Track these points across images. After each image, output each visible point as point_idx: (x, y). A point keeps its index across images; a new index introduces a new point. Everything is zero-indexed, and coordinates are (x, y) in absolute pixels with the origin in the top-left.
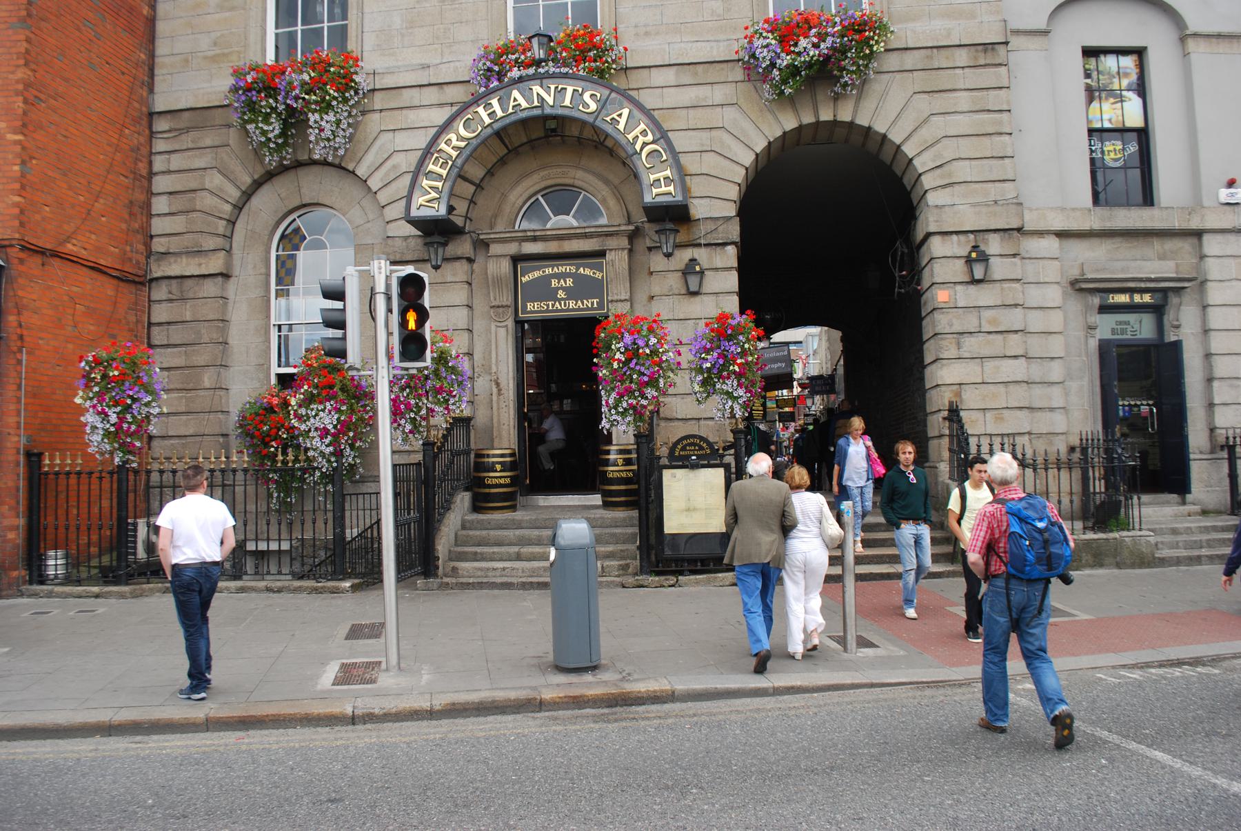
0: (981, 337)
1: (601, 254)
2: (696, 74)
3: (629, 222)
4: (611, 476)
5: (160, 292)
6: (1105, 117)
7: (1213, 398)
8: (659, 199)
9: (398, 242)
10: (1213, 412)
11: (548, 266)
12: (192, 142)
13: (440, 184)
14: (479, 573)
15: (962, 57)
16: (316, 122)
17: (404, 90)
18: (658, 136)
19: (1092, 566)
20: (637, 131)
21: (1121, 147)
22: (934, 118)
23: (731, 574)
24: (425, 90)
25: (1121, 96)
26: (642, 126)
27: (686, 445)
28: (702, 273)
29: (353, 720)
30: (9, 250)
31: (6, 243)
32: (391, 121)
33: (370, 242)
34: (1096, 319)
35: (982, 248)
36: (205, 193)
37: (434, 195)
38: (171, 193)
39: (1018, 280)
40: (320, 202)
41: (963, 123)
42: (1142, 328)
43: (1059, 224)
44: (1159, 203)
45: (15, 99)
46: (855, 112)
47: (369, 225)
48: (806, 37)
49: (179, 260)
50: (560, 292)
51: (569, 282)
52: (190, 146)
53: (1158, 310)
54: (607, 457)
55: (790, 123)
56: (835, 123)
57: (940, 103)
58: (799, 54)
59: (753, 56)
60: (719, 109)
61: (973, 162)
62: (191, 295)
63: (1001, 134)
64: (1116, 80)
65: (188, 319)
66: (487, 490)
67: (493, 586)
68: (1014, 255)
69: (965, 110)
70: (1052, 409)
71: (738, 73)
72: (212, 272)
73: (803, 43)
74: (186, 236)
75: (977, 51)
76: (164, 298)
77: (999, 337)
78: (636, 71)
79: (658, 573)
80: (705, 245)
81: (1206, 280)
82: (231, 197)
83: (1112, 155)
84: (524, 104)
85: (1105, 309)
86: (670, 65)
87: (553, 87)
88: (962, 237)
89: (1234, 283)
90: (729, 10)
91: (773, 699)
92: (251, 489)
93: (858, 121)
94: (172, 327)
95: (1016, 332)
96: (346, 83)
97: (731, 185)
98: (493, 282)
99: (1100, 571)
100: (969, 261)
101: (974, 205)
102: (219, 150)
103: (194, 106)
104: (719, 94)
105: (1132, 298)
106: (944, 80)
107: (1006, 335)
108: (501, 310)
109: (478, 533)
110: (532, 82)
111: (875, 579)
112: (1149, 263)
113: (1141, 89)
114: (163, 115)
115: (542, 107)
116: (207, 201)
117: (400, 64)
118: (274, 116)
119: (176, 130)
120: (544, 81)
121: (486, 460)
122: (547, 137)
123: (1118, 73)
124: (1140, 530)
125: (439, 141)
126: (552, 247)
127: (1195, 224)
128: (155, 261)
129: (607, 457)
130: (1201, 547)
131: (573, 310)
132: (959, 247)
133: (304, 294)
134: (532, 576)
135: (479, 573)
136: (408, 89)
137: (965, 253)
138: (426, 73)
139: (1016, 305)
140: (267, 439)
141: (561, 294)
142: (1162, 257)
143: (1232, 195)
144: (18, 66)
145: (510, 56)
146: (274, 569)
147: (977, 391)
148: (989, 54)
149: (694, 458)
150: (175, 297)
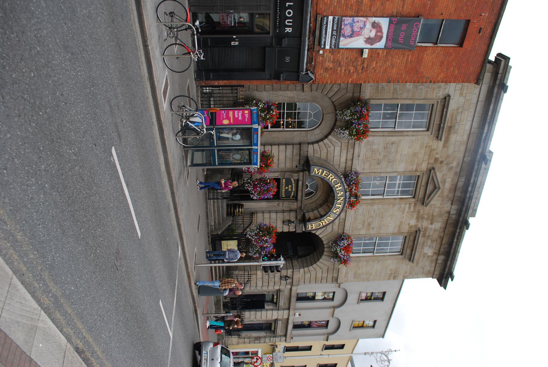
0: (268, 278)
2: (342, 222)
17: (353, 149)
22: (321, 270)
24: (352, 155)
26: (327, 222)
28: (288, 225)
37: (317, 172)
39: (280, 284)
40: (323, 121)
42: (268, 298)
47: (314, 136)
51: (290, 190)
53: (272, 301)
55: (325, 243)
60: (332, 227)
61: (309, 277)
68: (286, 284)
72: (304, 89)
77: (267, 281)
84: (338, 195)
87: (342, 202)
92: (231, 99)
100: (286, 276)
102: (346, 90)
113: (325, 299)
117: (362, 148)
125: (332, 173)
131: (282, 191)
141: (287, 188)
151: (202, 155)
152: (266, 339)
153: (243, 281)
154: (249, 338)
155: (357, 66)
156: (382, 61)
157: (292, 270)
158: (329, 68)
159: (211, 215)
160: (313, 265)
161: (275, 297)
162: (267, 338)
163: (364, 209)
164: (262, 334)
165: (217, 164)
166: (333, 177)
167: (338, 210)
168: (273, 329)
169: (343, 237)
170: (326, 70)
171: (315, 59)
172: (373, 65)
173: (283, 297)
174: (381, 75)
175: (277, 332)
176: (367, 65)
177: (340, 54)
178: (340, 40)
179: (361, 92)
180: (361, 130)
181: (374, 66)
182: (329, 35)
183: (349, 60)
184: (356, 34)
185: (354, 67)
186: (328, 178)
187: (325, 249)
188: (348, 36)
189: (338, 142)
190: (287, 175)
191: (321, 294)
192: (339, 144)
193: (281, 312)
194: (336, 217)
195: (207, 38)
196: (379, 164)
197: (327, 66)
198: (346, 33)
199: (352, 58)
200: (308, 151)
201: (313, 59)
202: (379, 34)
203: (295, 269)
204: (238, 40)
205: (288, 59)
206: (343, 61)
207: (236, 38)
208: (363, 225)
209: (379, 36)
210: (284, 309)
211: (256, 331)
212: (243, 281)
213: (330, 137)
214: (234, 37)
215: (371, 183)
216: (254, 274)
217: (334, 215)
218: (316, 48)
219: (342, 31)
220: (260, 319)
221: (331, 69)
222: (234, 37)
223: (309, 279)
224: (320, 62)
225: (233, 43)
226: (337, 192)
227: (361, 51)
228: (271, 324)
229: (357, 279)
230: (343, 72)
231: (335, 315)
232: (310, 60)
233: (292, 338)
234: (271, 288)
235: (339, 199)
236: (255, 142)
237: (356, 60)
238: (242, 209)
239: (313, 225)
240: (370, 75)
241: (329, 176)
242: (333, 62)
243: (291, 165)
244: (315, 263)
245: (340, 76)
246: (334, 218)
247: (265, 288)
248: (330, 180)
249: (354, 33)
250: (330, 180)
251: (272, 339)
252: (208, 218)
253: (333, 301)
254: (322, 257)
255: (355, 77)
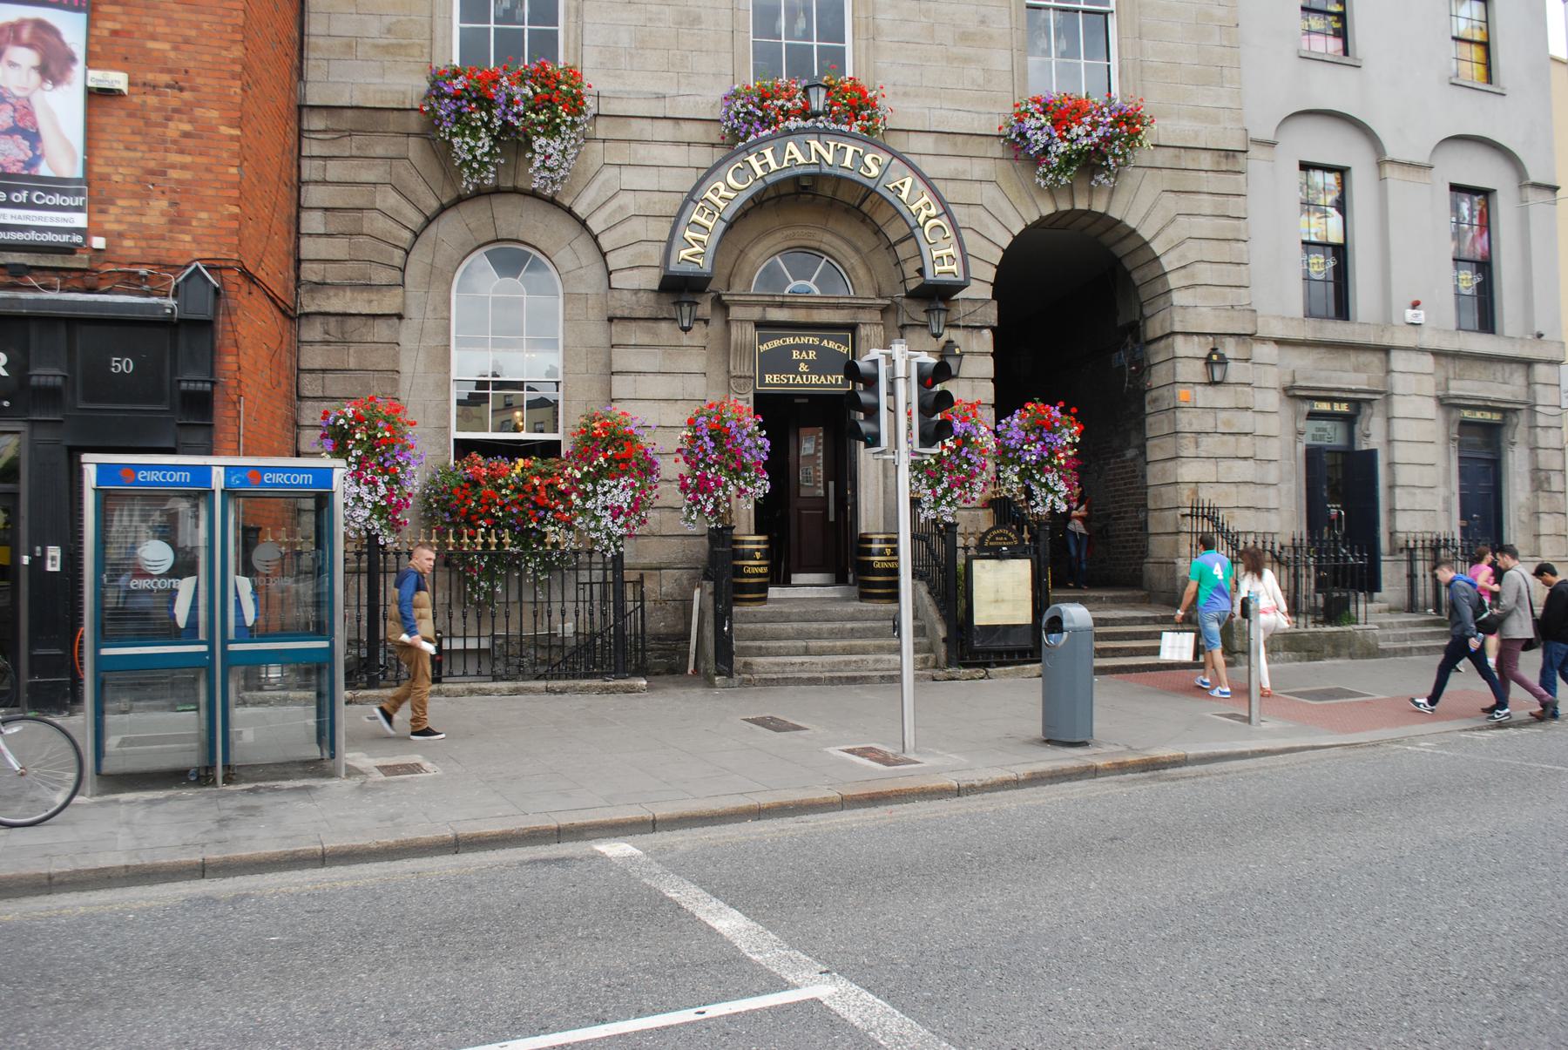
0: (1217, 438)
1: (852, 328)
2: (955, 144)
3: (880, 296)
4: (878, 566)
5: (313, 331)
6: (1313, 230)
7: (1394, 504)
8: (940, 278)
9: (627, 296)
10: (1395, 517)
11: (789, 336)
12: (358, 149)
13: (705, 238)
14: (776, 669)
15: (1206, 161)
16: (541, 146)
17: (633, 120)
18: (941, 211)
19: (1331, 657)
20: (919, 204)
21: (1323, 261)
22: (1180, 219)
23: (1038, 665)
25: (1326, 212)
26: (926, 199)
27: (995, 536)
28: (961, 356)
29: (959, 792)
30: (224, 273)
31: (223, 264)
32: (616, 153)
33: (583, 292)
34: (1302, 424)
35: (1221, 351)
36: (375, 214)
37: (698, 249)
38: (326, 209)
39: (1249, 384)
40: (521, 239)
41: (1205, 226)
42: (1333, 435)
43: (1279, 333)
44: (1356, 319)
45: (231, 83)
46: (1109, 203)
47: (582, 271)
48: (1080, 124)
49: (341, 293)
50: (802, 365)
51: (812, 355)
52: (355, 152)
53: (1349, 420)
54: (869, 546)
55: (1047, 209)
56: (1088, 213)
57: (1185, 204)
58: (1072, 141)
59: (1022, 135)
60: (977, 185)
61: (1215, 266)
62: (356, 338)
63: (1238, 240)
64: (1322, 196)
65: (352, 366)
66: (745, 580)
67: (798, 681)
68: (1247, 360)
69: (1208, 213)
70: (1268, 510)
71: (997, 149)
72: (387, 312)
73: (1077, 130)
74: (349, 264)
75: (1220, 156)
76: (318, 339)
77: (1232, 438)
78: (895, 133)
79: (966, 666)
80: (964, 327)
81: (1393, 394)
82: (411, 222)
83: (1316, 268)
84: (801, 160)
85: (1313, 416)
86: (930, 132)
87: (832, 144)
88: (1202, 339)
89: (1414, 398)
90: (990, 81)
91: (1255, 760)
93: (1111, 214)
94: (329, 376)
95: (1246, 434)
96: (575, 104)
97: (989, 266)
98: (736, 349)
99: (1338, 661)
100: (1208, 361)
101: (1215, 308)
103: (361, 104)
104: (978, 169)
105: (1332, 406)
106: (1190, 181)
107: (1237, 437)
108: (742, 380)
109: (752, 626)
110: (809, 136)
111: (1161, 670)
112: (1345, 375)
113: (1341, 205)
114: (316, 111)
115: (819, 164)
116: (379, 224)
117: (628, 88)
118: (484, 130)
119: (334, 131)
120: (822, 136)
121: (741, 547)
122: (797, 193)
123: (1324, 189)
124: (1366, 623)
125: (703, 188)
126: (800, 316)
127: (1386, 341)
128: (307, 292)
129: (869, 546)
130: (1406, 640)
131: (816, 385)
132: (1199, 348)
133: (493, 346)
134: (832, 671)
135: (776, 669)
136: (639, 120)
137: (1205, 355)
138: (662, 103)
139: (1247, 408)
140: (473, 517)
141: (803, 367)
142: (1357, 369)
143: (1416, 316)
144: (234, 42)
145: (775, 102)
146: (458, 671)
147: (1211, 490)
148: (1230, 160)
149: (1004, 548)
150: (333, 339)
151: (561, 692)
152: (1542, 444)
153: (1194, 535)
154: (1536, 515)
155: (166, 110)
156: (145, 20)
157: (1179, 340)
158: (172, 211)
159: (853, 667)
160: (1153, 252)
161: (1325, 407)
162: (1536, 441)
163: (893, 63)
164: (1516, 464)
165: (325, 644)
166: (933, 212)
167: (868, 159)
168: (1496, 417)
169: (1013, 136)
170: (177, 221)
171: (131, 264)
172: (164, 51)
173: (1323, 374)
174: (209, 18)
175: (1509, 397)
176: (162, 71)
177: (109, 175)
178: (52, 174)
179: (401, 107)
180: (535, 93)
181: (166, 46)
182: (27, 217)
183: (138, 138)
184: (22, 118)
185: (168, 119)
186: (722, 205)
187: (1081, 204)
188: (33, 148)
189: (601, 178)
190: (742, 367)
191: (1313, 220)
192: (610, 172)
193: (1399, 383)
194: (901, 164)
195: (32, 658)
196: (696, 20)
197: (163, 220)
198: (22, 157)
199: (128, 130)
200: (636, 291)
201: (129, 272)
202: (26, 34)
203: (1172, 324)
204: (38, 549)
205: (122, 365)
206: (142, 163)
207: (31, 553)
208: (967, 60)
209: (34, 35)
210: (1389, 371)
211: (1504, 485)
212: (1194, 535)
213: (579, 209)
214: (26, 560)
215: (787, 45)
216: (1195, 492)
217: (892, 174)
218: (80, 261)
219: (14, 169)
220: (1440, 469)
221: (174, 204)
222: (26, 560)
223: (1224, 266)
224: (143, 244)
225: (53, 565)
226: (785, 164)
227: (96, 96)
228: (1464, 424)
229: (1226, 71)
230: (188, 159)
231: (1422, 159)
232: (131, 281)
233: (1540, 336)
234: (1272, 425)
235: (820, 156)
236: (186, 476)
237: (139, 113)
238: (870, 541)
239: (935, 254)
240: (207, 58)
241: (716, 199)
242: (146, 196)
243: (695, 351)
244: (1146, 244)
245: (208, 170)
246: (908, 172)
247: (1273, 449)
248: (732, 195)
249: (21, 125)
250: (732, 195)
251: (1541, 420)
252: (862, 678)
253: (1348, 169)
254: (1118, 217)
255: (215, 114)
